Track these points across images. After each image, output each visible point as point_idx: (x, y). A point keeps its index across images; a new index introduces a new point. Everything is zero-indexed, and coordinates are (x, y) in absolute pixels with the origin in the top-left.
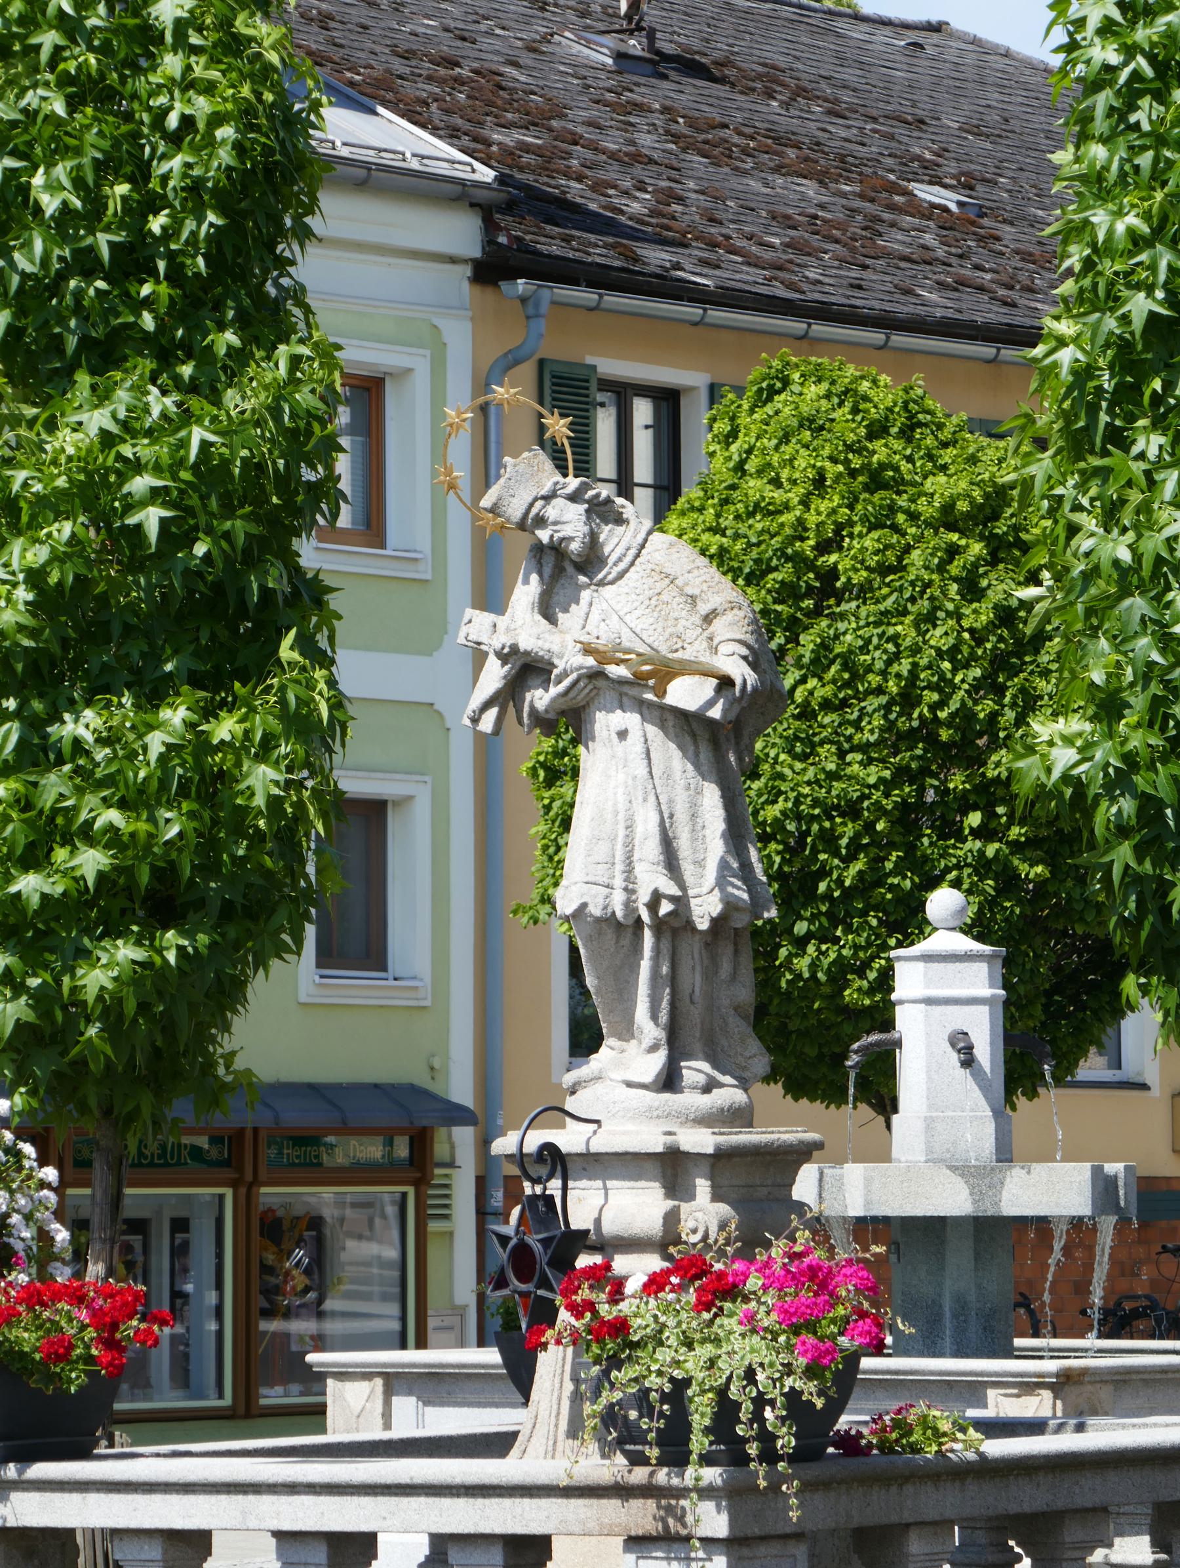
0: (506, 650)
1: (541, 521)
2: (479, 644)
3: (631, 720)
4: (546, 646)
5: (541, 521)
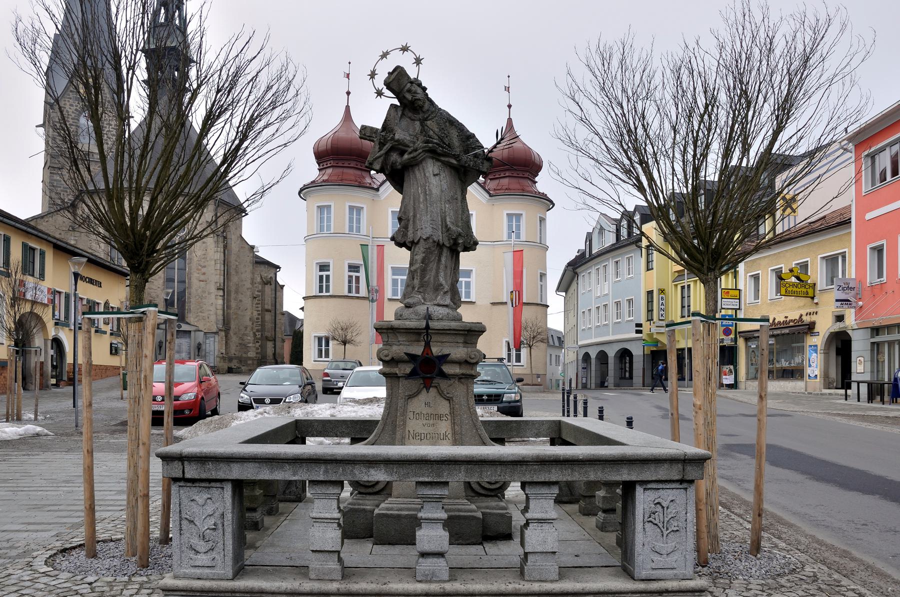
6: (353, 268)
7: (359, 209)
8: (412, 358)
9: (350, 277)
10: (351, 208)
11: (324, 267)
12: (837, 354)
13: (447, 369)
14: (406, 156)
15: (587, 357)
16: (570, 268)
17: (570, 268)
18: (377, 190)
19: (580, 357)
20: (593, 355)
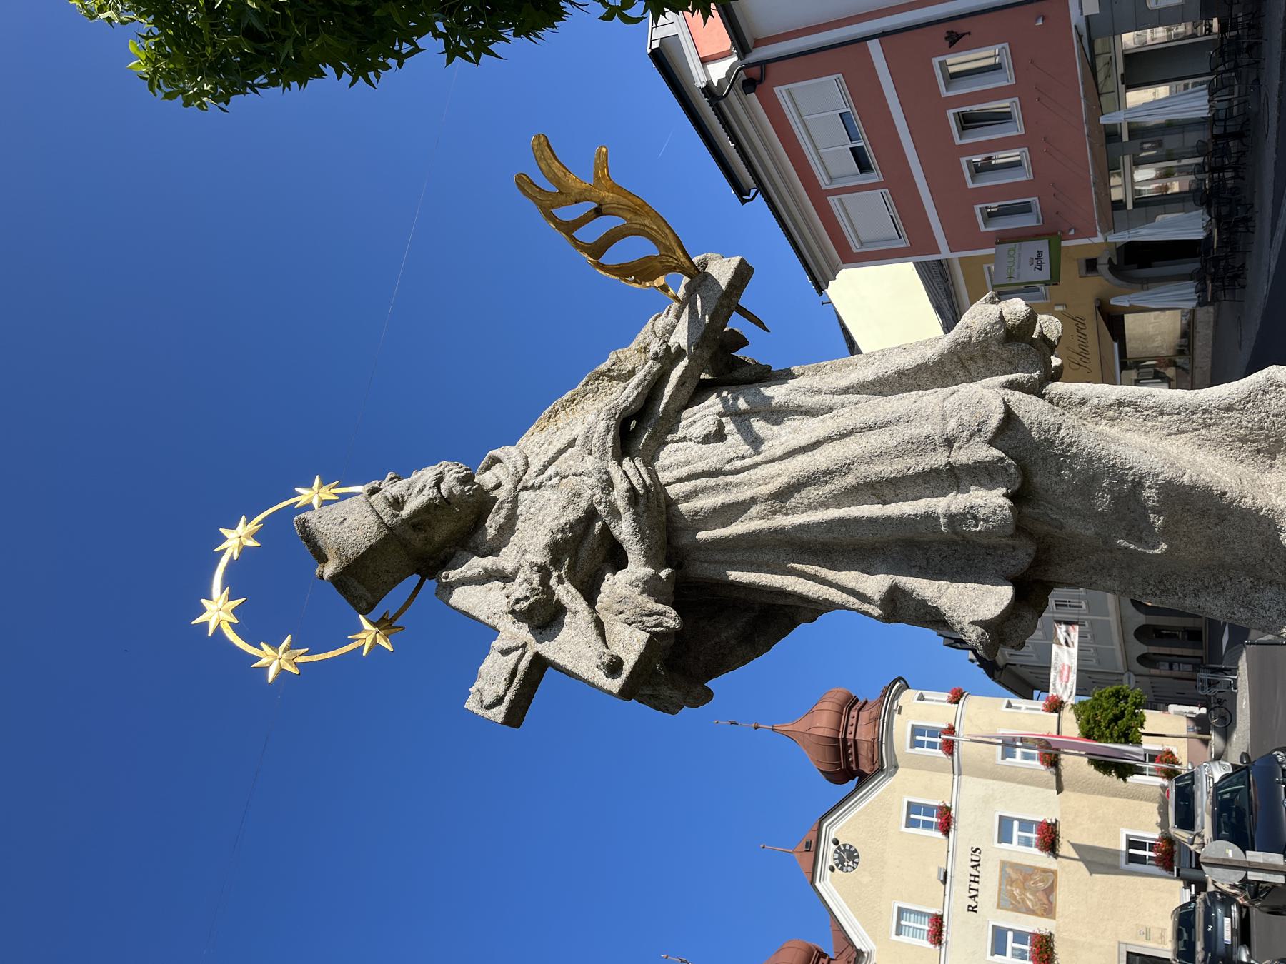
0: (536, 578)
1: (397, 503)
2: (513, 673)
4: (557, 511)
5: (397, 503)
11: (972, 909)
12: (1150, 267)
14: (625, 530)
15: (1143, 659)
16: (997, 674)
17: (997, 674)
18: (860, 953)
19: (1144, 670)
20: (1142, 649)
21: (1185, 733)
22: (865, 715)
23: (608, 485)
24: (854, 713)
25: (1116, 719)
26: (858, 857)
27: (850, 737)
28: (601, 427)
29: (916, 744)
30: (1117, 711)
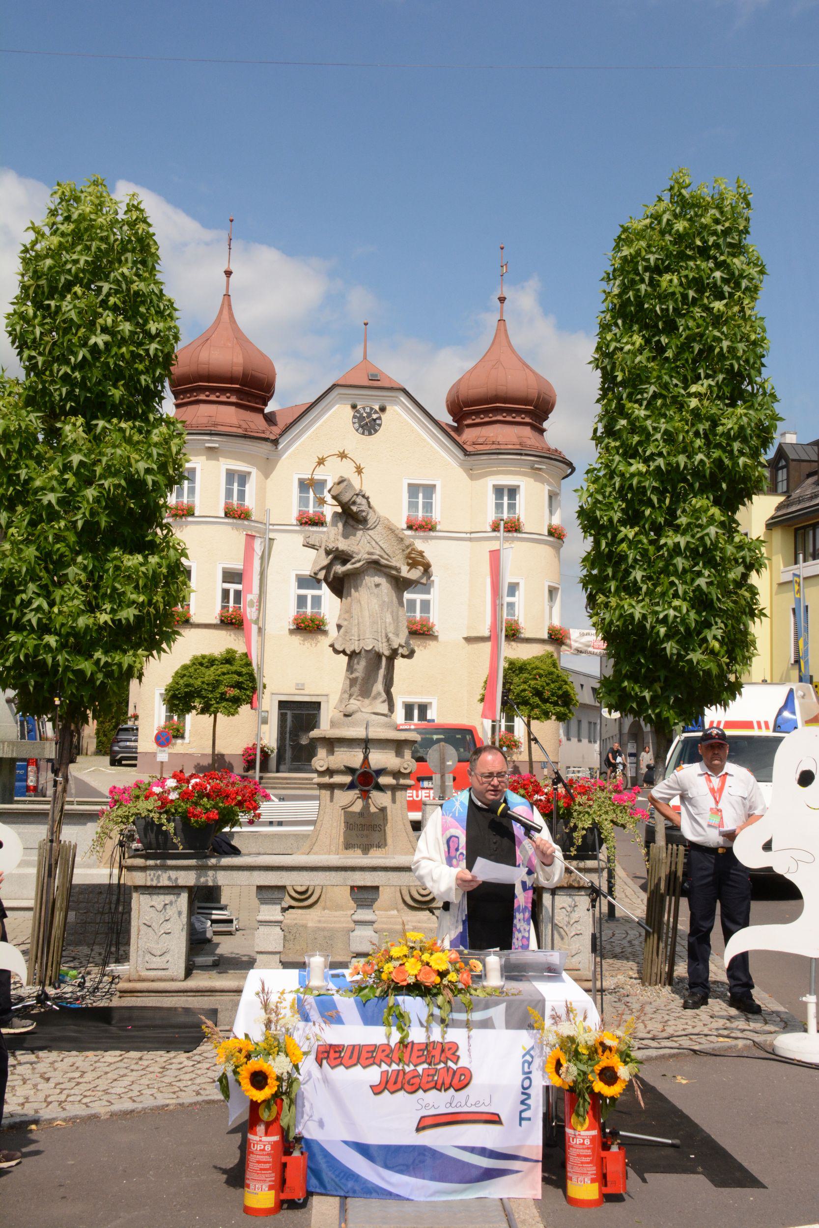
1: (354, 503)
3: (382, 580)
5: (354, 503)
6: (230, 576)
7: (513, 492)
8: (350, 770)
9: (226, 593)
10: (499, 491)
13: (383, 780)
14: (349, 566)
18: (275, 442)
21: (534, 759)
22: (527, 431)
23: (359, 561)
24: (233, 399)
25: (538, 693)
26: (370, 434)
27: (202, 397)
28: (375, 557)
29: (499, 491)
30: (547, 694)
